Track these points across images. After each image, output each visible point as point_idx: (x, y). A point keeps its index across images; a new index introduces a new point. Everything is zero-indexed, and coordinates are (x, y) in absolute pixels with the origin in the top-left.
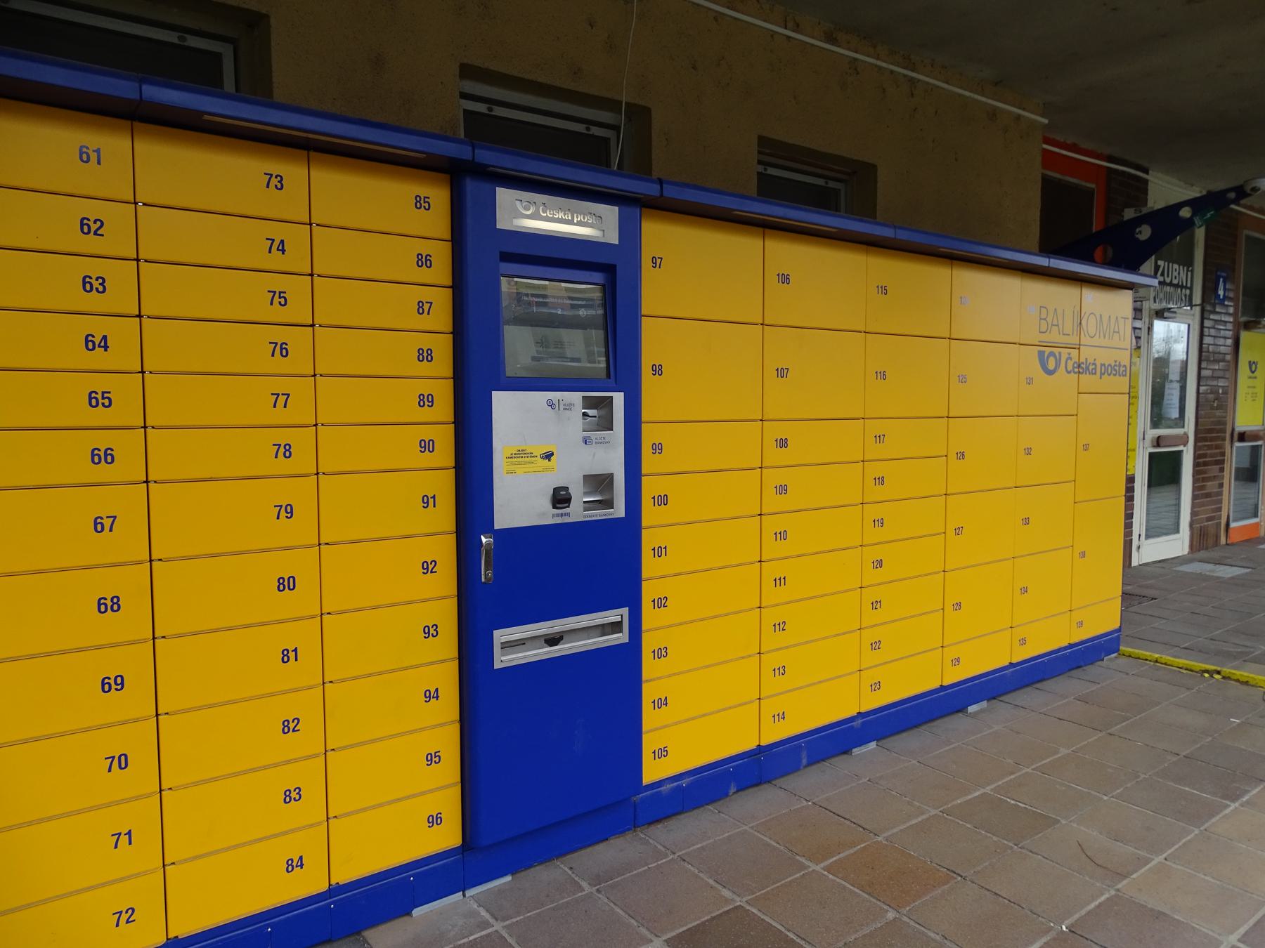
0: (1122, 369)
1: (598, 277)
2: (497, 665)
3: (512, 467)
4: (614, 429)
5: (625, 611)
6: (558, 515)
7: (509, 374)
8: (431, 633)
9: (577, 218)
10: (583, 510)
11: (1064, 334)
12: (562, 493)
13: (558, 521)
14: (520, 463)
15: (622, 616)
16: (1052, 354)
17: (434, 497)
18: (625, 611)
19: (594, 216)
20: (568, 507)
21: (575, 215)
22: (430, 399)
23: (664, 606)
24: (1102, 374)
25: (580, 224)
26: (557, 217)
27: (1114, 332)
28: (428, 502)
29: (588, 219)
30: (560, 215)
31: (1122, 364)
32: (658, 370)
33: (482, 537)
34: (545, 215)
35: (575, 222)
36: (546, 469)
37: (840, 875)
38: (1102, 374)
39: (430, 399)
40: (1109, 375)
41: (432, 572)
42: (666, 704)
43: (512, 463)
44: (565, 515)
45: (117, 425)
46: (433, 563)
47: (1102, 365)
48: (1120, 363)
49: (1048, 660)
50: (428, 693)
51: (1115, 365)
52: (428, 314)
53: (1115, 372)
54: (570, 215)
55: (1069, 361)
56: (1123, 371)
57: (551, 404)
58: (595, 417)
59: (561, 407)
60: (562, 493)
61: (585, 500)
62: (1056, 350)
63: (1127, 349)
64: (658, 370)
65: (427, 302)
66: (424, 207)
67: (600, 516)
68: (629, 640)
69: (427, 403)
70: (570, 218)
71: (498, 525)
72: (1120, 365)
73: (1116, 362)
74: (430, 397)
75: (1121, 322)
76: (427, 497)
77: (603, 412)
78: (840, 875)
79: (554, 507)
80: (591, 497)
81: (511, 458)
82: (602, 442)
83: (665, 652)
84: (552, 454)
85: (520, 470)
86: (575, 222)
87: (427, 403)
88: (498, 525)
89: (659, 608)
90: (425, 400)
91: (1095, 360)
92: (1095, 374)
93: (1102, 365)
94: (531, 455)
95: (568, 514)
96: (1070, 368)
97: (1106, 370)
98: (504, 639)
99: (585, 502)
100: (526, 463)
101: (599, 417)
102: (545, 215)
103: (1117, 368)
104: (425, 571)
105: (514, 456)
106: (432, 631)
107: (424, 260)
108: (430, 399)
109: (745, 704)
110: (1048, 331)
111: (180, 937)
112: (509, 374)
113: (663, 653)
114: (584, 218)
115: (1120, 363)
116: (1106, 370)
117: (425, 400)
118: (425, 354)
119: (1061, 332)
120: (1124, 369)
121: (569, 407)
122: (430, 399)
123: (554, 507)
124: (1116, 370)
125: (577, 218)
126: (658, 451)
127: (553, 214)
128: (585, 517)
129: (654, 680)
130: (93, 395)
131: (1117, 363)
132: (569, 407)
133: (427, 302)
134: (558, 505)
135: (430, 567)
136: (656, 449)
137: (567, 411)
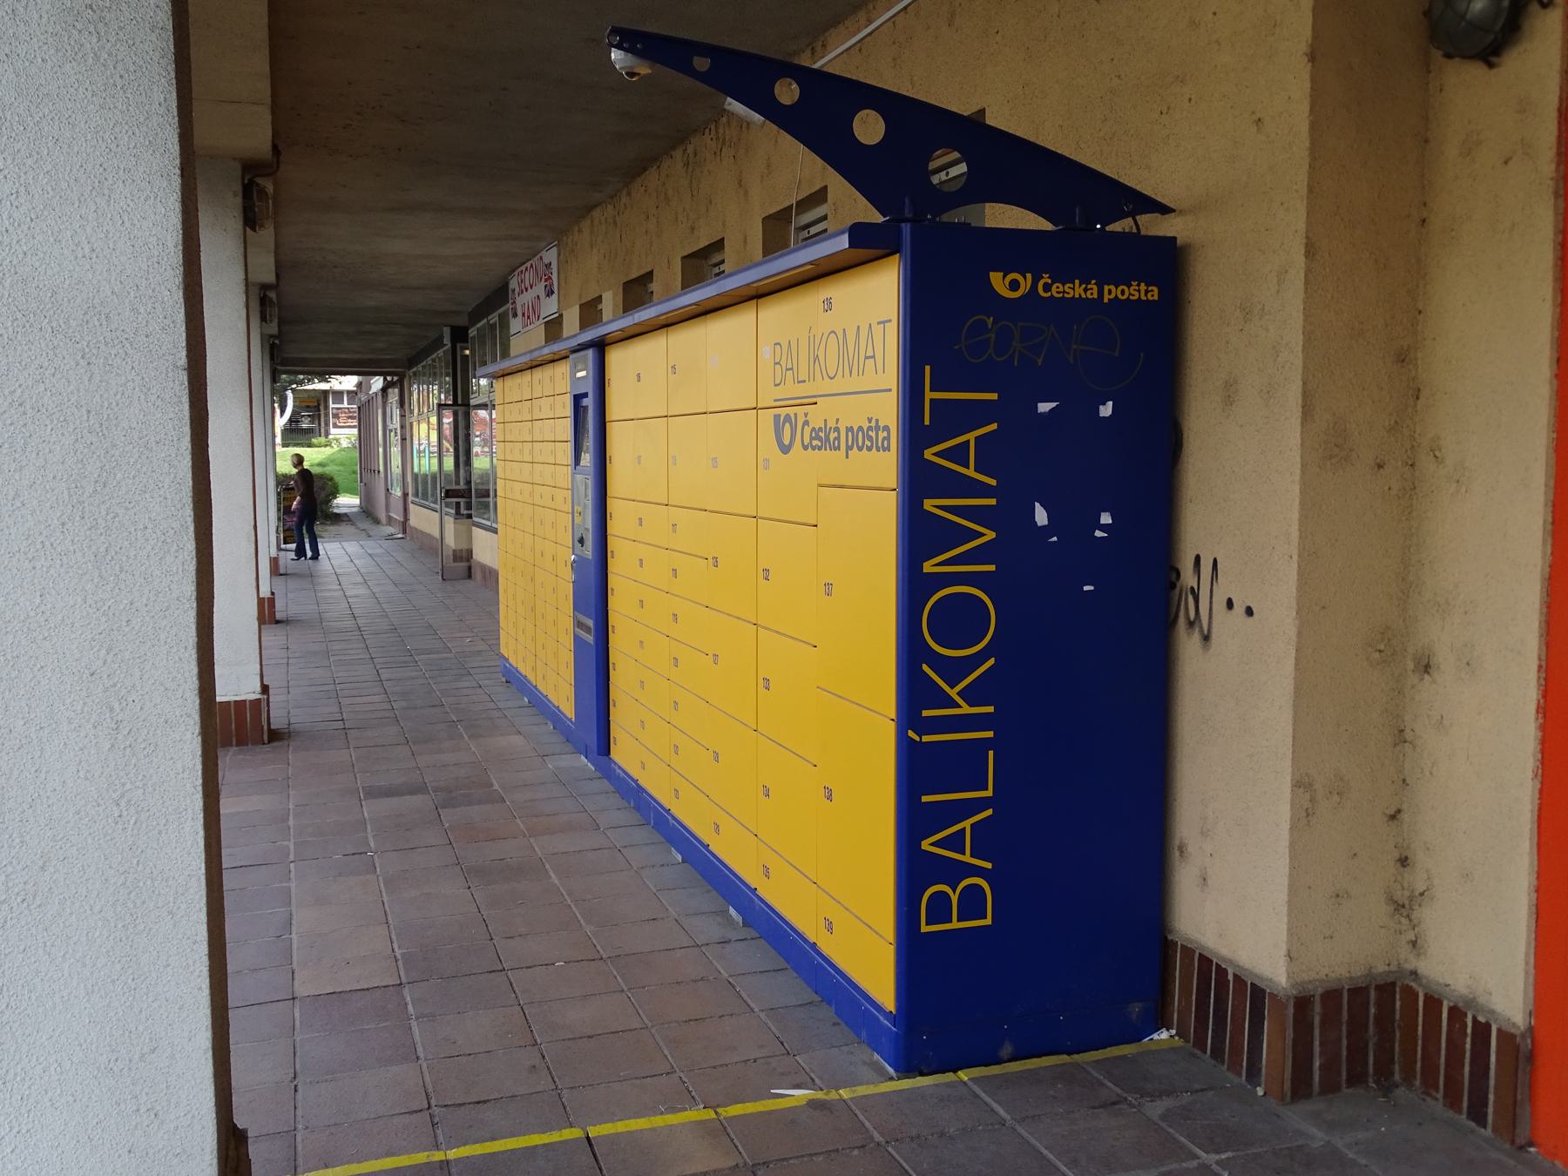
0: (882, 435)
11: (799, 382)
12: (1091, 588)
16: (788, 416)
24: (849, 448)
27: (866, 358)
31: (881, 424)
34: (1049, 294)
37: (1007, 1050)
38: (849, 448)
40: (860, 449)
47: (849, 429)
48: (877, 421)
49: (624, 779)
51: (870, 428)
53: (869, 443)
55: (806, 427)
56: (884, 439)
60: (1091, 588)
62: (790, 411)
63: (890, 390)
72: (877, 428)
73: (870, 420)
75: (878, 330)
78: (1007, 1050)
91: (838, 420)
92: (838, 448)
93: (849, 429)
96: (807, 441)
97: (855, 439)
102: (1049, 294)
103: (873, 434)
109: (797, 755)
110: (783, 383)
111: (1531, 1008)
115: (877, 421)
116: (855, 439)
119: (796, 380)
120: (885, 434)
124: (870, 439)
131: (873, 424)
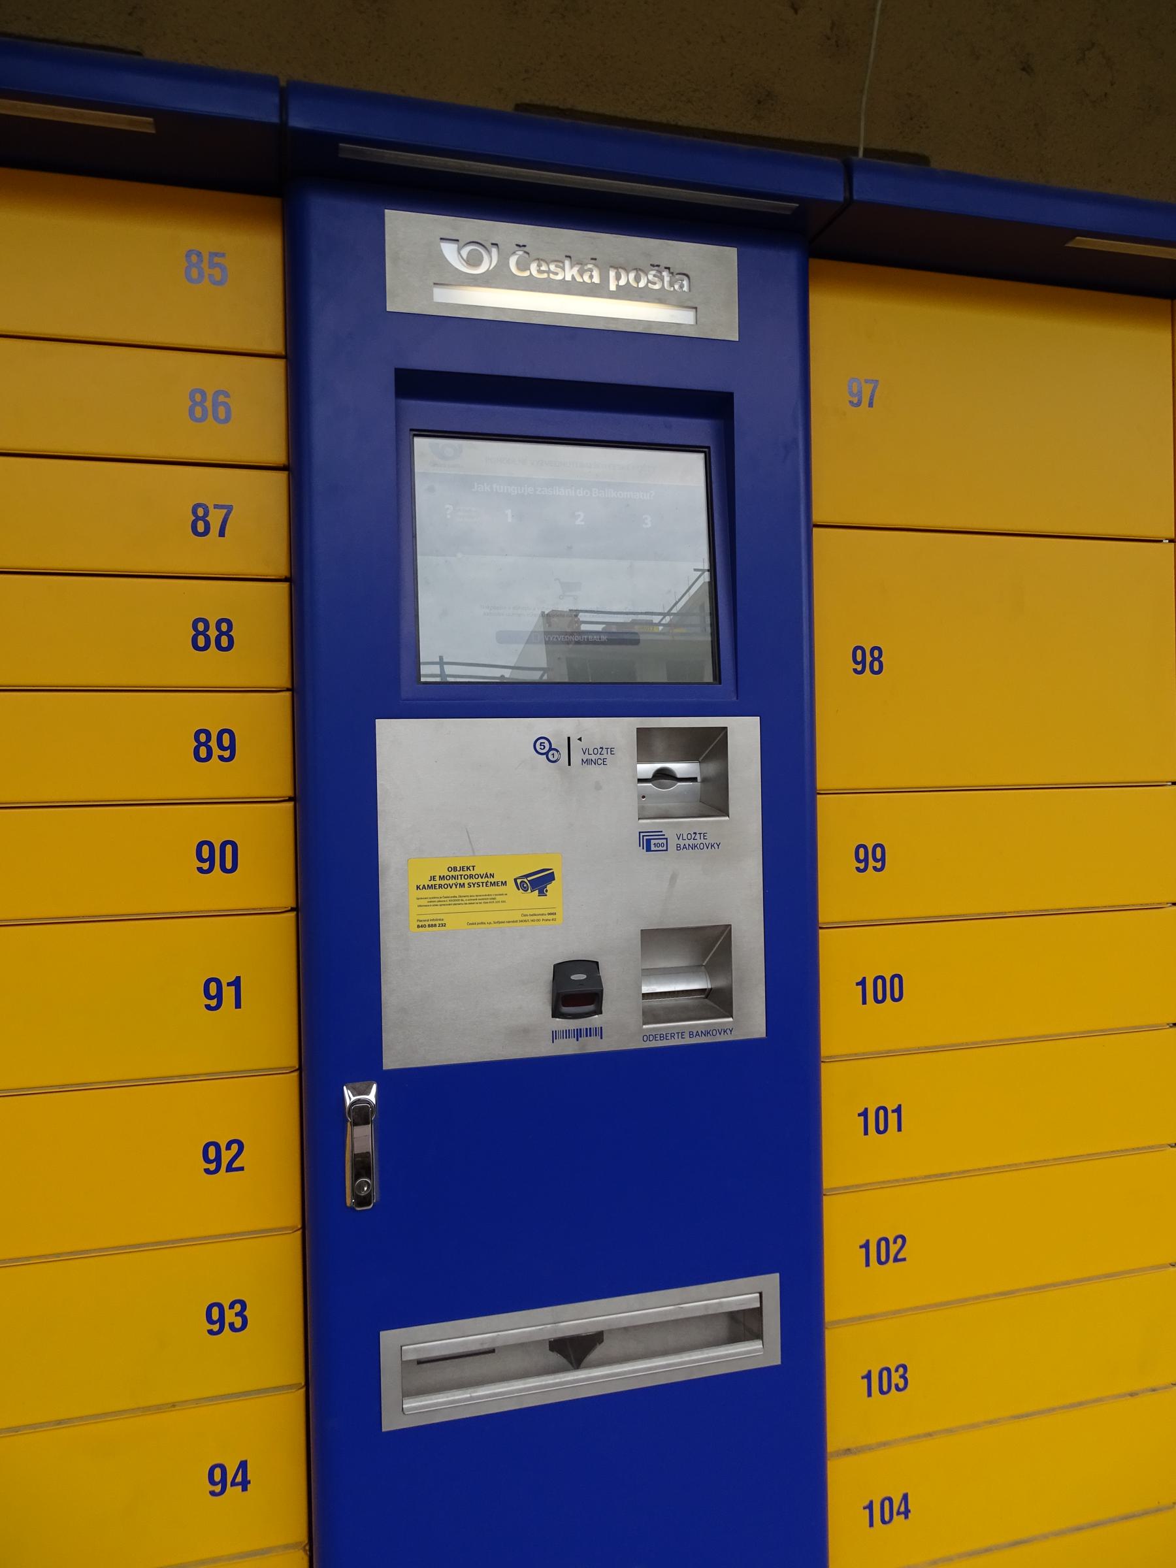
1: (701, 428)
2: (391, 1422)
3: (431, 913)
4: (732, 809)
5: (771, 1283)
6: (567, 1034)
7: (429, 672)
8: (227, 1321)
9: (618, 278)
10: (639, 1017)
13: (569, 1047)
14: (455, 900)
15: (761, 1294)
17: (236, 983)
18: (771, 1283)
19: (665, 274)
20: (599, 1011)
21: (612, 274)
22: (226, 742)
23: (896, 1260)
25: (625, 293)
26: (559, 277)
28: (219, 996)
29: (649, 281)
30: (569, 273)
32: (869, 659)
33: (345, 1088)
34: (527, 274)
35: (613, 287)
36: (535, 917)
39: (226, 741)
41: (230, 1168)
42: (906, 1513)
43: (433, 902)
44: (589, 1032)
45: (893, 785)
46: (235, 1147)
50: (218, 1472)
52: (222, 533)
54: (596, 274)
57: (545, 748)
58: (694, 779)
59: (577, 757)
60: (574, 977)
61: (646, 989)
64: (869, 659)
65: (216, 506)
66: (210, 276)
67: (691, 1034)
68: (782, 1362)
69: (216, 751)
70: (596, 280)
71: (392, 1060)
74: (226, 737)
76: (218, 982)
77: (712, 768)
79: (556, 1014)
80: (688, 982)
81: (430, 887)
82: (695, 844)
83: (903, 1377)
84: (550, 877)
85: (456, 919)
86: (613, 287)
87: (216, 751)
88: (392, 1060)
89: (880, 1262)
90: (213, 743)
94: (489, 881)
95: (599, 1032)
98: (413, 1351)
99: (646, 996)
100: (472, 900)
101: (704, 780)
102: (527, 274)
104: (212, 1167)
105: (438, 882)
106: (230, 1316)
107: (209, 404)
108: (226, 742)
112: (429, 672)
113: (896, 1379)
114: (637, 280)
117: (213, 743)
118: (213, 633)
121: (598, 756)
122: (226, 741)
123: (556, 1014)
125: (618, 278)
126: (871, 863)
127: (549, 272)
128: (647, 1037)
129: (869, 1448)
130: (227, 754)
132: (598, 756)
133: (216, 506)
134: (565, 1009)
135: (226, 1156)
136: (866, 860)
137: (592, 767)
